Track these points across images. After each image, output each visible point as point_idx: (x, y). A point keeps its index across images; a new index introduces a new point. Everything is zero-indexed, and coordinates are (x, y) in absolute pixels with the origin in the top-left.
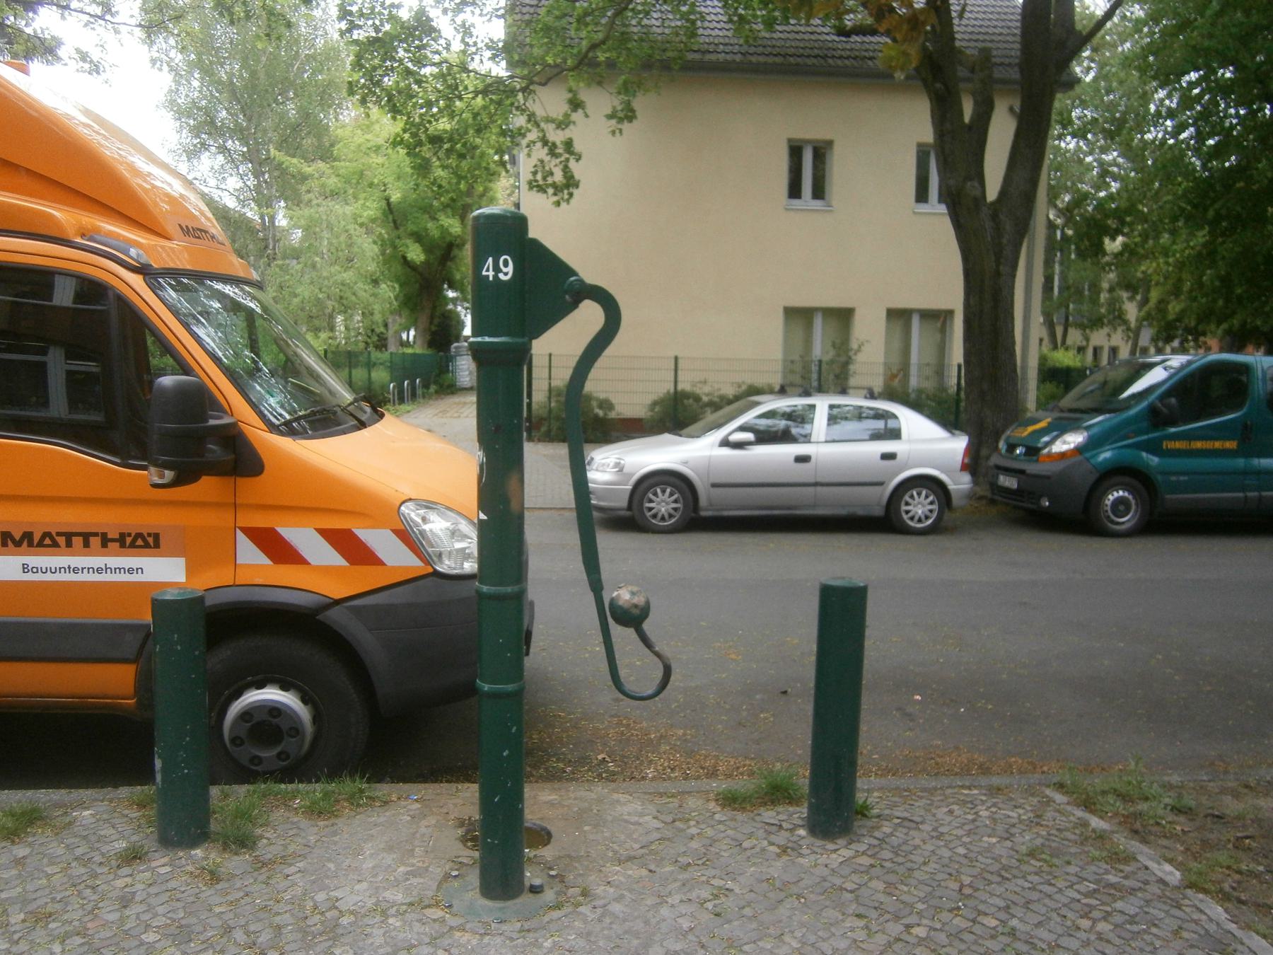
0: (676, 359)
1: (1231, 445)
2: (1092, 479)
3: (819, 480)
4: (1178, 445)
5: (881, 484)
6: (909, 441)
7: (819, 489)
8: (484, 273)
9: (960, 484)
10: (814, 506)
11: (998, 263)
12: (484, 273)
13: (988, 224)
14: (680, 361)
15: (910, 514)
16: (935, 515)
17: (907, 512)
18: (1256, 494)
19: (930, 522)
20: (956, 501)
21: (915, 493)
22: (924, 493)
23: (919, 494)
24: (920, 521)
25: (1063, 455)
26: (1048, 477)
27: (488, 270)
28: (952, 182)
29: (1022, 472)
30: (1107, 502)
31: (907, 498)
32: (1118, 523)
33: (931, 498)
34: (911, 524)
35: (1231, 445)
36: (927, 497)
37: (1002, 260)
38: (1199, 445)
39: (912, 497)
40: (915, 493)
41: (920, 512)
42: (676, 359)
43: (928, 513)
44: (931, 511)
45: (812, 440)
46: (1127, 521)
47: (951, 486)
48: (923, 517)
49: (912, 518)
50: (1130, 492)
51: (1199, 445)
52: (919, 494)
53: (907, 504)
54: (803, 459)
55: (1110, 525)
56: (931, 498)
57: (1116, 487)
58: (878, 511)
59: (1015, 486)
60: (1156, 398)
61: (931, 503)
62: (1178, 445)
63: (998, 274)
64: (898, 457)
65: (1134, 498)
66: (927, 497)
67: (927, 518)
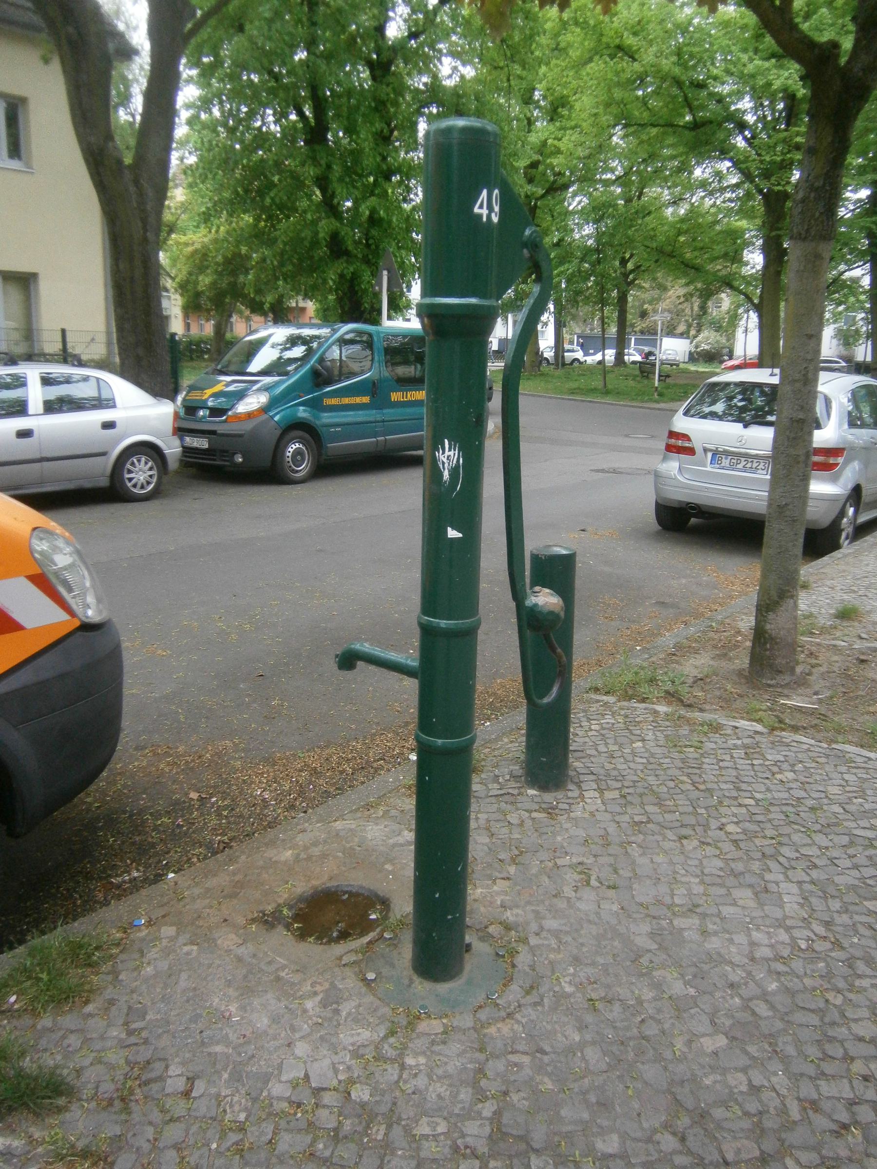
0: (63, 332)
1: (366, 400)
2: (278, 432)
3: (44, 455)
4: (334, 401)
5: (103, 454)
6: (125, 408)
7: (45, 464)
8: (476, 210)
9: (172, 448)
10: (42, 483)
11: (145, 230)
12: (476, 210)
13: (132, 189)
14: (68, 334)
15: (133, 482)
16: (155, 480)
17: (130, 480)
18: (383, 438)
19: (151, 486)
20: (173, 464)
21: (135, 461)
22: (143, 459)
23: (139, 461)
24: (142, 487)
25: (250, 415)
26: (241, 436)
27: (481, 207)
28: (93, 139)
29: (213, 432)
30: (288, 454)
31: (128, 466)
32: (297, 472)
33: (150, 464)
34: (135, 491)
35: (366, 400)
36: (146, 463)
37: (148, 228)
38: (346, 401)
39: (133, 464)
40: (135, 461)
41: (142, 478)
42: (63, 332)
43: (149, 479)
44: (151, 476)
45: (31, 412)
46: (304, 468)
47: (167, 451)
48: (145, 484)
49: (135, 486)
50: (304, 445)
51: (346, 401)
52: (139, 461)
53: (130, 472)
54: (24, 434)
55: (296, 475)
56: (150, 464)
57: (291, 441)
58: (104, 482)
59: (206, 446)
60: (316, 362)
61: (151, 469)
62: (334, 401)
63: (145, 240)
64: (118, 424)
65: (307, 449)
66: (146, 463)
67: (148, 483)
